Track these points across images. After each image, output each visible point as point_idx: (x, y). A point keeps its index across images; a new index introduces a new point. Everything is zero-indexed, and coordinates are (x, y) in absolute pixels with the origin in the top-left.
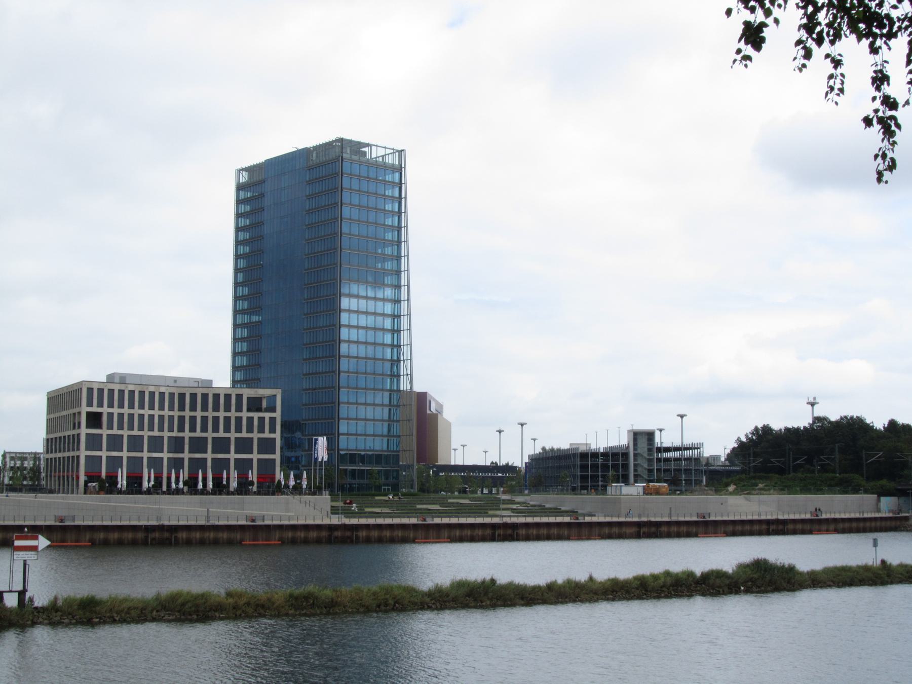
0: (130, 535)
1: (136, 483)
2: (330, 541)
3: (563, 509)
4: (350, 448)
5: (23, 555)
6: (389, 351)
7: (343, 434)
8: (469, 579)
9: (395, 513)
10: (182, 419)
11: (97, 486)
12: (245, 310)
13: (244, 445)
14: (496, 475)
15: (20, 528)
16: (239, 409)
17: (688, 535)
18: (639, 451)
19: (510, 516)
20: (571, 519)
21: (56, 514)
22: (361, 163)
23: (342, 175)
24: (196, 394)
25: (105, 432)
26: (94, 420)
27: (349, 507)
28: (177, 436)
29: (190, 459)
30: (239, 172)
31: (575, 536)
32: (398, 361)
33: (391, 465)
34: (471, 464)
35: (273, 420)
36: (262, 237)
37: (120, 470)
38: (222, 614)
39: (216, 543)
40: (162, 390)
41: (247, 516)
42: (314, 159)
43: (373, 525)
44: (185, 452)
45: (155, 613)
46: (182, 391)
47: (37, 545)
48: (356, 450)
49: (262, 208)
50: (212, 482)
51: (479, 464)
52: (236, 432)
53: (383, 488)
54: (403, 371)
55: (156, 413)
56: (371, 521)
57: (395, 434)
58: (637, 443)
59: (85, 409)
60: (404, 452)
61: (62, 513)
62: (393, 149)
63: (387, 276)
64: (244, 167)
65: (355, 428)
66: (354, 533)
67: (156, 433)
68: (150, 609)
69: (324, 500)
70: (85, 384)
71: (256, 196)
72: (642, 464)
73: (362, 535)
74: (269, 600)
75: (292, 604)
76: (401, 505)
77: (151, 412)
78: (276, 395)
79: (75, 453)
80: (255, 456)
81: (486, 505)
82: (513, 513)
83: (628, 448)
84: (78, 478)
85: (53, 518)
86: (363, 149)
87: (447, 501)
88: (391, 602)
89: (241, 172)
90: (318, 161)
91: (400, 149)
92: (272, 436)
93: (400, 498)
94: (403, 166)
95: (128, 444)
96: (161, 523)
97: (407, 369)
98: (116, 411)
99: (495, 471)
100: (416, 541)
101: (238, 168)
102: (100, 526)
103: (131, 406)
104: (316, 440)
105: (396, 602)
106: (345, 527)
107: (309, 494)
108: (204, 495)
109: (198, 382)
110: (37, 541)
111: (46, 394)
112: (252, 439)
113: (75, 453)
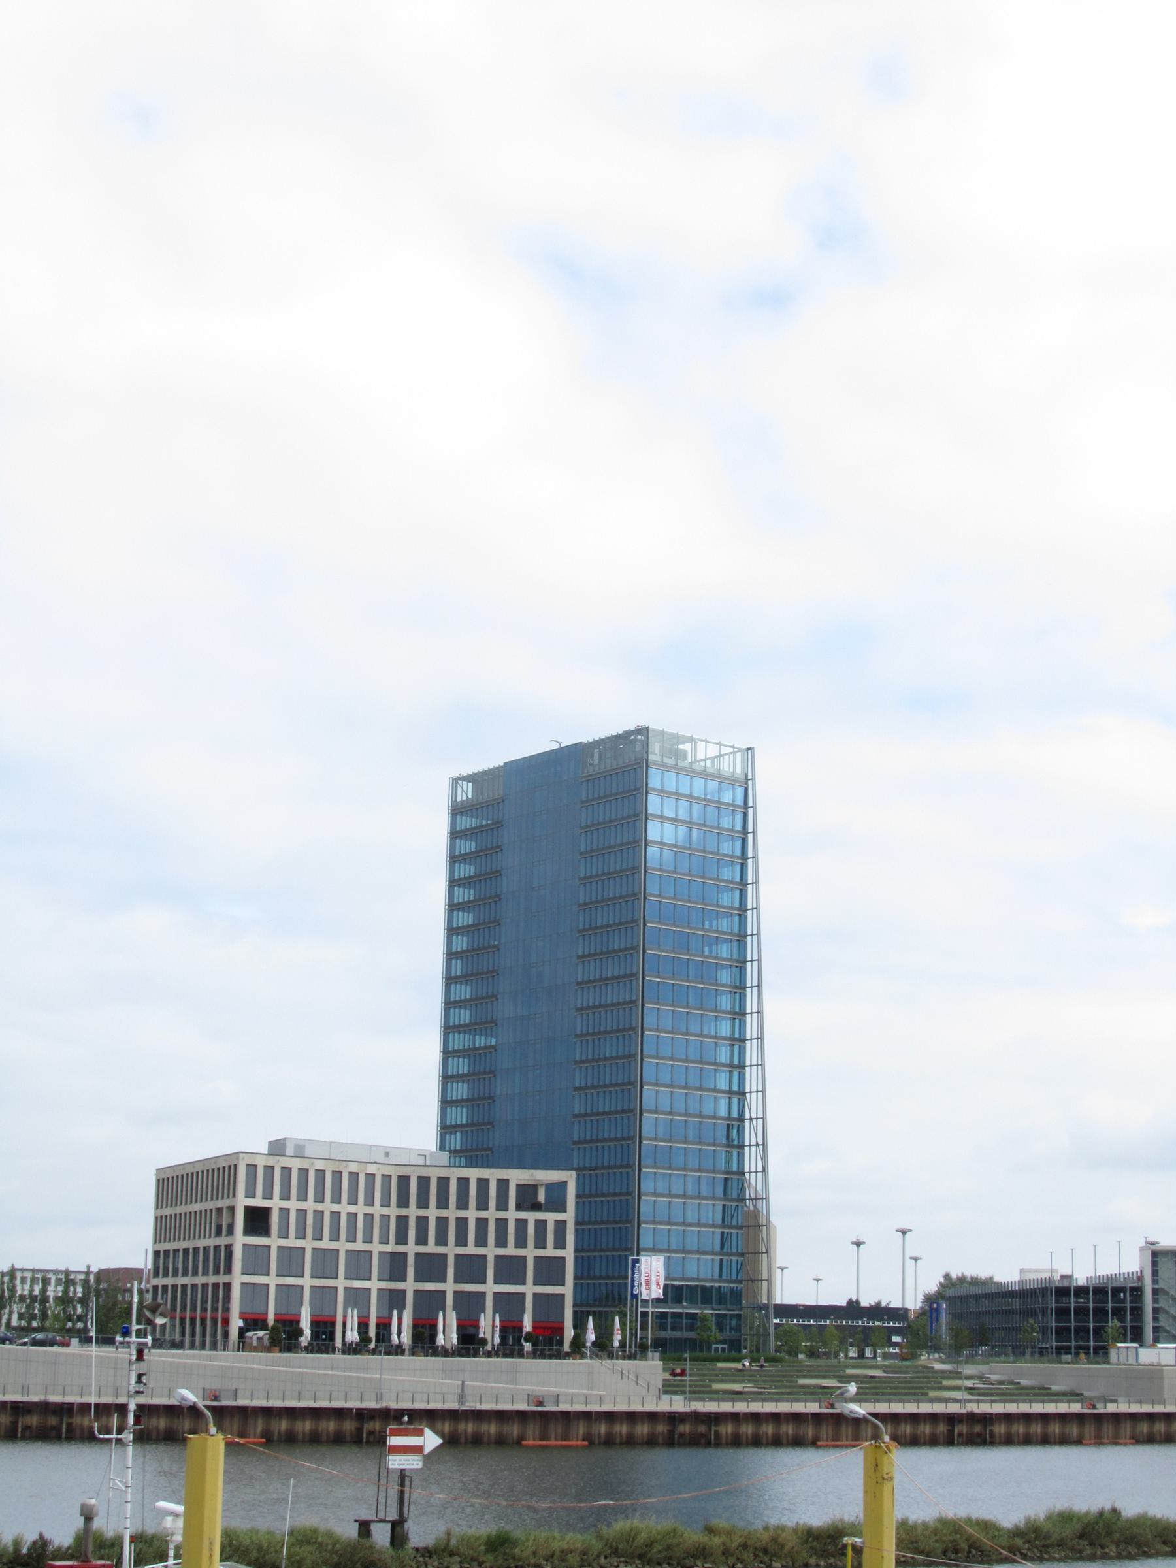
0: (331, 1426)
1: (324, 1333)
2: (671, 1442)
3: (1055, 1388)
4: (702, 1276)
5: (400, 1460)
8: (846, 1518)
9: (769, 1393)
10: (402, 1221)
11: (267, 1337)
13: (510, 1269)
14: (855, 1324)
15: (397, 1415)
16: (502, 1205)
17: (1064, 1441)
18: (1161, 1285)
20: (1082, 1408)
21: (207, 1387)
24: (428, 1179)
25: (274, 1242)
26: (258, 1220)
28: (394, 1251)
29: (456, 1293)
30: (457, 784)
31: (1090, 1439)
32: (741, 1119)
34: (827, 1304)
35: (561, 1226)
36: (497, 898)
38: (706, 1563)
40: (371, 1169)
42: (596, 762)
44: (408, 1279)
45: (602, 1560)
46: (404, 1172)
47: (421, 1444)
48: (698, 1279)
50: (457, 1334)
51: (839, 1305)
53: (714, 1346)
54: (749, 1137)
55: (361, 1209)
56: (726, 1407)
58: (1157, 1270)
59: (242, 1202)
61: (213, 1384)
62: (733, 747)
63: (722, 969)
64: (465, 774)
65: (711, 1241)
66: (713, 1429)
67: (359, 1245)
68: (596, 1553)
69: (653, 1367)
70: (243, 1158)
71: (487, 825)
72: (1167, 1309)
73: (727, 1433)
74: (775, 1540)
75: (812, 1548)
76: (912, 1385)
77: (352, 1209)
79: (222, 1279)
80: (529, 1289)
81: (914, 1380)
82: (971, 1394)
83: (1140, 1278)
84: (226, 1321)
86: (681, 747)
88: (964, 1546)
89: (460, 782)
91: (745, 747)
92: (559, 1253)
94: (750, 777)
95: (379, 1268)
96: (384, 1405)
97: (756, 1134)
98: (293, 1205)
99: (886, 1318)
100: (819, 1443)
101: (456, 774)
103: (320, 1198)
104: (637, 1261)
105: (970, 1547)
106: (696, 1417)
107: (624, 1358)
110: (422, 1438)
111: (155, 1172)
112: (485, 1257)
113: (222, 1279)
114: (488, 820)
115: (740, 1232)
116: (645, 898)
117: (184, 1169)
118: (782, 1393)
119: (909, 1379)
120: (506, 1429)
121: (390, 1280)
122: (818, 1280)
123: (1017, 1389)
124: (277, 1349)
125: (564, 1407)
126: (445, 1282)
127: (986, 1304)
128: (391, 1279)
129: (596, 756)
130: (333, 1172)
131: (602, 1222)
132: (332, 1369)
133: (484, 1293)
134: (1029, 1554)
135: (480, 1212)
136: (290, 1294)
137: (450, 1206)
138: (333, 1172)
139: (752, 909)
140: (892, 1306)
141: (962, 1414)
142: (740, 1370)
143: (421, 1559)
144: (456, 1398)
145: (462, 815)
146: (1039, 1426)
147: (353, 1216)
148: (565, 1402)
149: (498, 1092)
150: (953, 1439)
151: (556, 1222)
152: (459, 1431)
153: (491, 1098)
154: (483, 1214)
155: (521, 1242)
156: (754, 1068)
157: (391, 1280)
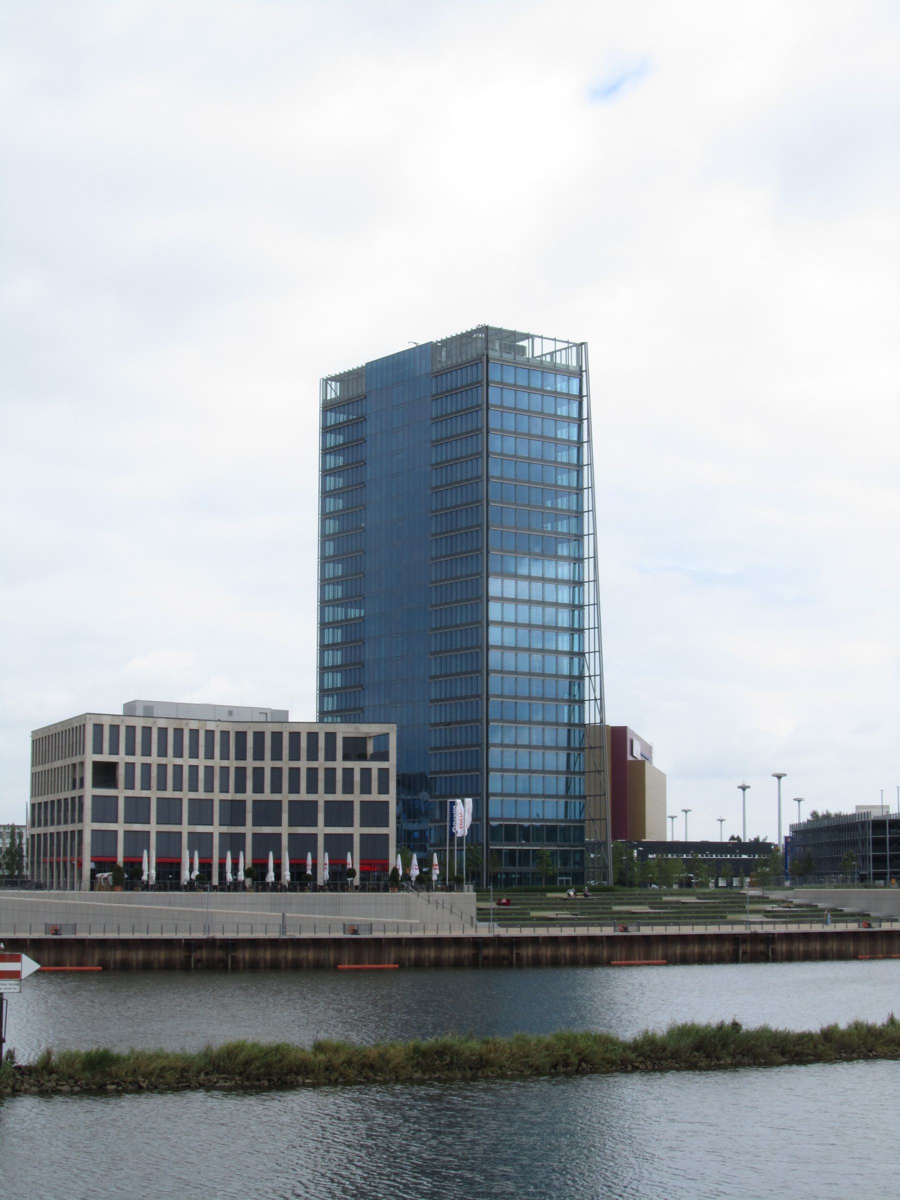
1: (171, 873)
2: (476, 963)
3: (846, 910)
6: (565, 661)
7: (495, 795)
9: (579, 919)
10: (241, 772)
11: (110, 878)
16: (330, 755)
17: (842, 956)
19: (762, 923)
20: (859, 927)
25: (121, 793)
30: (327, 383)
32: (581, 677)
34: (699, 841)
35: (384, 773)
37: (145, 852)
38: (307, 1078)
39: (296, 966)
40: (210, 726)
41: (344, 925)
42: (444, 359)
45: (202, 1076)
46: (241, 728)
47: (19, 969)
51: (710, 841)
53: (559, 878)
55: (201, 762)
56: (541, 932)
59: (90, 757)
61: (54, 920)
62: (568, 342)
64: (334, 375)
66: (515, 952)
67: (201, 794)
71: (353, 419)
74: (382, 1056)
77: (194, 762)
78: (388, 734)
79: (76, 827)
80: (356, 830)
84: (80, 865)
85: (43, 927)
86: (521, 343)
87: (661, 899)
88: (574, 1060)
89: (329, 382)
91: (579, 342)
92: (383, 798)
93: (586, 895)
94: (584, 369)
96: (211, 935)
97: (594, 690)
98: (138, 759)
99: (738, 851)
100: (613, 962)
101: (325, 376)
103: (163, 753)
105: (581, 1061)
106: (499, 941)
107: (442, 890)
114: (353, 415)
115: (582, 777)
116: (488, 480)
117: (56, 728)
118: (591, 919)
119: (717, 905)
120: (323, 955)
121: (231, 825)
122: (721, 821)
123: (811, 911)
124: (119, 888)
125: (377, 934)
126: (281, 825)
127: (825, 838)
128: (232, 824)
129: (444, 354)
130: (175, 729)
131: (456, 772)
132: (170, 904)
133: (316, 835)
134: (641, 1066)
135: (239, 761)
136: (137, 841)
137: (284, 757)
138: (175, 729)
139: (588, 488)
140: (767, 841)
141: (746, 935)
142: (565, 899)
143: (19, 1077)
144: (277, 928)
145: (331, 412)
146: (835, 944)
147: (194, 769)
148: (378, 931)
149: (367, 659)
150: (738, 956)
151: (380, 769)
152: (280, 958)
153: (362, 664)
154: (313, 764)
155: (348, 788)
156: (592, 631)
157: (232, 825)
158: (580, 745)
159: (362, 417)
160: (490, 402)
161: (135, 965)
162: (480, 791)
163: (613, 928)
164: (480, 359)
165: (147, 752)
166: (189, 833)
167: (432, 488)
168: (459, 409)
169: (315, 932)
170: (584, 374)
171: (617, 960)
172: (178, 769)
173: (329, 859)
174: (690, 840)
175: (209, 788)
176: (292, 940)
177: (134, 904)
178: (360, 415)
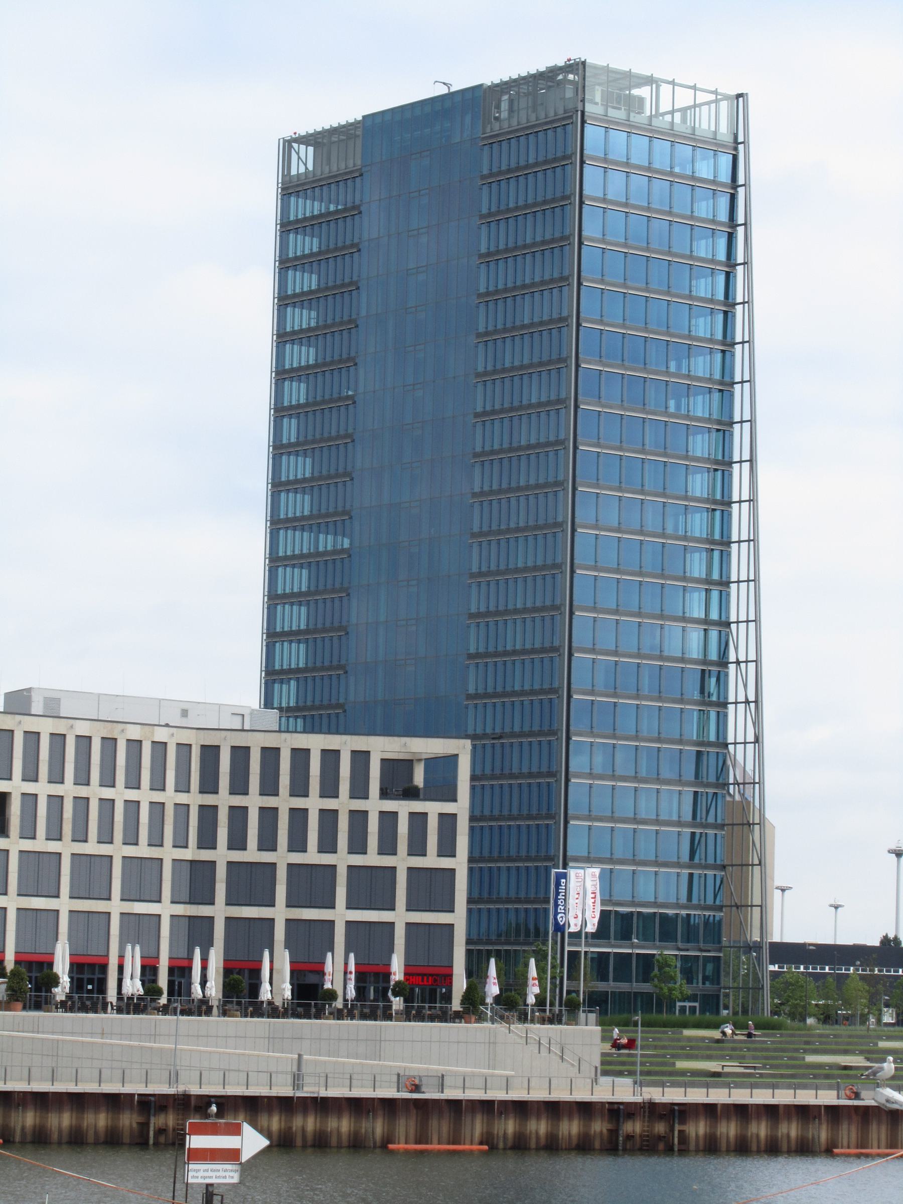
0: (101, 1120)
1: (90, 981)
5: (207, 1170)
6: (695, 636)
9: (761, 1075)
10: (208, 814)
12: (303, 518)
16: (359, 790)
22: (630, 129)
23: (582, 162)
27: (629, 1055)
30: (291, 147)
32: (723, 662)
33: (680, 944)
34: (851, 943)
35: (448, 822)
37: (266, 954)
40: (161, 735)
41: (399, 1075)
42: (504, 115)
43: (724, 1105)
47: (239, 1147)
49: (352, 246)
50: (291, 984)
52: (350, 852)
53: (678, 1004)
54: (735, 690)
55: (145, 796)
56: (696, 1096)
57: (711, 861)
60: (734, 909)
62: (715, 92)
64: (303, 133)
66: (677, 1127)
67: (143, 850)
71: (337, 212)
73: (697, 1136)
77: (132, 795)
78: (457, 755)
86: (636, 92)
87: (876, 1044)
89: (295, 145)
90: (514, 122)
91: (734, 92)
92: (446, 863)
93: (750, 1035)
94: (740, 139)
96: (181, 1089)
97: (745, 686)
98: (43, 789)
100: (836, 1150)
101: (288, 134)
102: (25, 1093)
103: (83, 779)
106: (652, 1110)
108: (278, 1017)
109: (243, 715)
122: (836, 907)
124: (20, 1005)
129: (504, 106)
131: (511, 818)
139: (743, 343)
149: (354, 620)
153: (344, 629)
154: (330, 804)
155: (388, 846)
158: (718, 779)
159: (354, 208)
160: (586, 192)
161: (55, 1137)
162: (552, 853)
163: (835, 1093)
164: (571, 117)
165: (57, 777)
166: (288, 921)
167: (479, 335)
168: (530, 201)
169: (100, 1082)
170: (741, 147)
171: (842, 1148)
172: (108, 805)
173: (356, 964)
174: (839, 942)
175: (157, 841)
176: (315, 1099)
177: (43, 1033)
178: (349, 205)
